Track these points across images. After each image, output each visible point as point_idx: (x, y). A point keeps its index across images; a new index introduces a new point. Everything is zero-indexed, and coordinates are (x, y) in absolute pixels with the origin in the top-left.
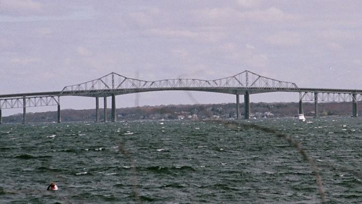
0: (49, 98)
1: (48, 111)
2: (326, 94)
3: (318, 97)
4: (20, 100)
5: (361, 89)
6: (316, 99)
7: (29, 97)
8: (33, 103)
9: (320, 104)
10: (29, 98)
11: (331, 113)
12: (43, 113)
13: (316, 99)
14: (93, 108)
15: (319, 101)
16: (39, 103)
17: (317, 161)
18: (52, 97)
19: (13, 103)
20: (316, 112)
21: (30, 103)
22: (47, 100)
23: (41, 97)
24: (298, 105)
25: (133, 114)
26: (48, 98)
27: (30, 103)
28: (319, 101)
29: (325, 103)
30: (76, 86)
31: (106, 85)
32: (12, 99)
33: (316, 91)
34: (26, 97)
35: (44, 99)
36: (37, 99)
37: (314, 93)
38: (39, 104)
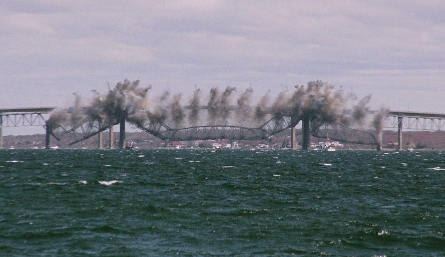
0: (35, 116)
3: (403, 123)
6: (400, 125)
9: (405, 134)
11: (421, 145)
13: (400, 125)
18: (39, 114)
20: (399, 143)
23: (23, 115)
26: (33, 115)
28: (404, 129)
29: (415, 133)
31: (39, 111)
32: (15, 115)
33: (400, 115)
36: (19, 117)
37: (397, 118)
38: (21, 123)
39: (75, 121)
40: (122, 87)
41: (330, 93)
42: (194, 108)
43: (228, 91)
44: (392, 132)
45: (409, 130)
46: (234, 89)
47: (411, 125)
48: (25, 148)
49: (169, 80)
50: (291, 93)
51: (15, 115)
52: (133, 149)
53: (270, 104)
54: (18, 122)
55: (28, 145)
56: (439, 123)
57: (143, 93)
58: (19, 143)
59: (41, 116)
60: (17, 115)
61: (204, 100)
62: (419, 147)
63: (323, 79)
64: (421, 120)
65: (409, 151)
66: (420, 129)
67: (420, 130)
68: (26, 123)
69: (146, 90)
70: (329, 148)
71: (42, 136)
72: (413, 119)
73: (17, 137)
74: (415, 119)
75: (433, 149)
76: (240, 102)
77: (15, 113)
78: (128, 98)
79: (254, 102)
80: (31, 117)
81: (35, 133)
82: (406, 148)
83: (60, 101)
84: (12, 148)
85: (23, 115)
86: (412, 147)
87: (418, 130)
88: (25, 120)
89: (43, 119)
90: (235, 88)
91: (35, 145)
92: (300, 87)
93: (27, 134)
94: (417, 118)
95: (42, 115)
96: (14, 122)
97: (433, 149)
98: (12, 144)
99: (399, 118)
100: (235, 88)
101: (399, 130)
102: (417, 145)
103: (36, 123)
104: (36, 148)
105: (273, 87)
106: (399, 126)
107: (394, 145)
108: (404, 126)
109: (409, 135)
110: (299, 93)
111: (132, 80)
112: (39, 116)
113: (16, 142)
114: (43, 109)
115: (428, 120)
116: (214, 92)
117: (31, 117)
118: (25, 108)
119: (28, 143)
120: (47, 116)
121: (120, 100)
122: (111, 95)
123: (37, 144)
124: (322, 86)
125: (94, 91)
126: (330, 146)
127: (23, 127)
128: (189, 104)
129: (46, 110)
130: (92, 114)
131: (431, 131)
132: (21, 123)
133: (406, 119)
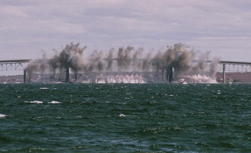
0: (17, 64)
3: (226, 68)
4: (13, 64)
6: (224, 69)
8: (5, 68)
9: (227, 74)
11: (236, 80)
12: (14, 76)
13: (224, 69)
17: (182, 88)
18: (20, 63)
19: (8, 67)
20: (223, 79)
23: (11, 64)
25: (120, 104)
26: (17, 64)
27: (11, 68)
28: (227, 71)
29: (233, 73)
30: (8, 70)
31: (20, 61)
32: (7, 64)
33: (224, 63)
35: (14, 65)
36: (8, 65)
37: (222, 65)
38: (9, 69)
39: (43, 67)
40: (69, 48)
41: (194, 50)
42: (110, 61)
43: (129, 49)
44: (220, 72)
45: (229, 72)
46: (132, 48)
47: (230, 69)
48: (12, 83)
49: (93, 47)
50: (164, 50)
51: (7, 64)
52: (74, 83)
53: (153, 56)
54: (17, 67)
55: (14, 81)
56: (238, 67)
57: (81, 52)
58: (9, 80)
59: (21, 64)
60: (8, 64)
61: (115, 55)
62: (235, 81)
63: (183, 42)
64: (236, 66)
65: (229, 83)
66: (235, 71)
67: (236, 72)
68: (13, 69)
69: (83, 50)
70: (183, 82)
71: (23, 75)
72: (231, 65)
73: (8, 76)
74: (241, 65)
75: (243, 82)
76: (135, 56)
77: (7, 63)
78: (72, 54)
79: (143, 56)
80: (16, 65)
81: (18, 74)
82: (228, 82)
83: (34, 55)
84: (5, 83)
85: (11, 64)
86: (231, 81)
87: (231, 72)
88: (3, 68)
89: (22, 66)
90: (133, 47)
91: (18, 81)
92: (170, 47)
93: (14, 75)
94: (233, 65)
95: (22, 64)
96: (6, 68)
97: (243, 82)
98: (5, 81)
99: (223, 65)
100: (133, 47)
101: (223, 71)
102: (234, 81)
103: (19, 68)
104: (19, 83)
105: (154, 46)
106: (223, 70)
107: (221, 80)
108: (226, 69)
109: (229, 74)
110: (169, 51)
111: (75, 43)
112: (20, 64)
113: (7, 80)
114: (243, 63)
115: (240, 66)
116: (121, 50)
117: (16, 65)
118: (6, 60)
119: (13, 80)
120: (25, 65)
121: (68, 56)
122: (63, 54)
123: (19, 80)
124: (182, 47)
125: (54, 50)
126: (184, 81)
127: (11, 71)
128: (106, 57)
129: (27, 61)
130: (53, 64)
131: (242, 72)
132: (9, 69)
133: (227, 65)
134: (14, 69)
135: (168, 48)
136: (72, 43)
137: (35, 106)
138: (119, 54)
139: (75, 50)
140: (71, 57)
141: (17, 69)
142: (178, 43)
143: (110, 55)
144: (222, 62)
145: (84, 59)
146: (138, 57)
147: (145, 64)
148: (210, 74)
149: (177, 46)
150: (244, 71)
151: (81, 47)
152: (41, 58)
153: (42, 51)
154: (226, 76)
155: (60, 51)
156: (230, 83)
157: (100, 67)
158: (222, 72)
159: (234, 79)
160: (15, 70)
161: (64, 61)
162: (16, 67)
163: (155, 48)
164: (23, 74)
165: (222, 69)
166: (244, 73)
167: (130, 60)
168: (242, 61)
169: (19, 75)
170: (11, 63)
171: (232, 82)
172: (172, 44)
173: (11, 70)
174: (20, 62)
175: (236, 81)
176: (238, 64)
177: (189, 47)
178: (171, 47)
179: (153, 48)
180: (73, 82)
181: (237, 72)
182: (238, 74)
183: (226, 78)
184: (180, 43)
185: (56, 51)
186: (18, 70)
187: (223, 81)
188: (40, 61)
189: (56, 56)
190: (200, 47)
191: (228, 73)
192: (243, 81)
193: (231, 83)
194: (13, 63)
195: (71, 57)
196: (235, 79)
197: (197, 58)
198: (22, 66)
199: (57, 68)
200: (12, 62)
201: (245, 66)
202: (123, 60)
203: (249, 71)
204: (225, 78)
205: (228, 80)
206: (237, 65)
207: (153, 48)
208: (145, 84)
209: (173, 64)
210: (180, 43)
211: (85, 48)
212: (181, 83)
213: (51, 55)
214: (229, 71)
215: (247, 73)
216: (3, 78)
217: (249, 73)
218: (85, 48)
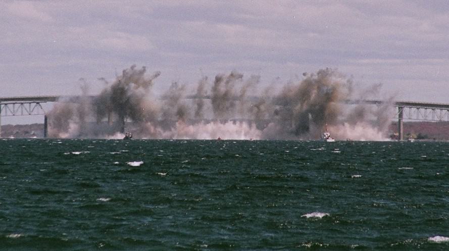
0: (33, 105)
1: (34, 122)
2: (431, 110)
5: (448, 103)
6: (401, 115)
7: (5, 102)
9: (405, 124)
10: (6, 104)
13: (401, 115)
14: (39, 122)
15: (405, 119)
16: (20, 110)
18: (38, 103)
19: (16, 109)
20: (400, 134)
21: (6, 112)
22: (30, 107)
23: (22, 104)
24: (43, 127)
27: (6, 112)
28: (405, 119)
29: (415, 123)
30: (17, 114)
31: (38, 100)
32: (30, 103)
33: (401, 105)
34: (2, 102)
36: (17, 105)
37: (397, 108)
38: (19, 113)
42: (198, 98)
47: (412, 115)
50: (297, 83)
51: (14, 104)
55: (27, 134)
57: (147, 84)
61: (208, 90)
62: (419, 137)
64: (422, 110)
67: (421, 121)
68: (25, 112)
70: (328, 139)
72: (414, 109)
73: (15, 126)
75: (434, 139)
76: (244, 91)
77: (14, 102)
78: (133, 90)
79: (259, 91)
82: (408, 138)
83: (65, 88)
86: (413, 138)
89: (42, 108)
91: (34, 135)
98: (11, 134)
99: (399, 108)
101: (400, 120)
102: (418, 136)
103: (35, 112)
104: (35, 137)
105: (278, 76)
106: (399, 117)
108: (405, 116)
109: (410, 125)
111: (139, 68)
112: (38, 105)
113: (15, 132)
115: (429, 110)
116: (218, 80)
117: (30, 106)
129: (53, 99)
131: (433, 121)
133: (406, 110)
134: (27, 113)
135: (305, 78)
136: (132, 68)
137: (26, 203)
138: (215, 89)
139: (136, 82)
140: (129, 94)
141: (32, 113)
142: (324, 68)
143: (200, 89)
144: (397, 103)
145: (153, 99)
146: (249, 93)
147: (258, 104)
148: (378, 124)
149: (323, 74)
150: (437, 119)
151: (147, 75)
152: (79, 93)
153: (82, 79)
154: (404, 128)
155: (113, 81)
156: (412, 141)
157: (181, 113)
158: (397, 120)
159: (418, 134)
160: (30, 114)
161: (119, 102)
162: (31, 110)
163: (279, 77)
164: (43, 122)
165: (398, 117)
166: (436, 123)
167: (235, 98)
168: (417, 101)
169: (36, 124)
170: (22, 102)
171: (415, 139)
172: (313, 70)
173: (22, 115)
174: (38, 101)
175: (423, 138)
176: (426, 107)
177: (345, 77)
178: (312, 75)
179: (278, 78)
180: (131, 137)
181: (425, 122)
182: (425, 125)
183: (404, 132)
184: (327, 69)
185: (107, 83)
186: (35, 115)
187: (399, 138)
188: (75, 99)
189: (106, 91)
190: (200, 70)
191: (407, 122)
192: (434, 137)
193: (412, 141)
194: (25, 102)
195: (129, 94)
196: (419, 135)
197: (355, 96)
198: (42, 108)
199: (139, 100)
200: (6, 101)
201: (438, 111)
202: (222, 102)
203: (446, 119)
204: (402, 132)
205: (408, 135)
206: (439, 110)
207: (278, 78)
208: (260, 145)
209: (314, 104)
210: (327, 69)
211: (157, 75)
212: (323, 140)
213: (97, 89)
214: (410, 119)
215: (441, 123)
216: (7, 129)
217: (445, 122)
218: (157, 75)
